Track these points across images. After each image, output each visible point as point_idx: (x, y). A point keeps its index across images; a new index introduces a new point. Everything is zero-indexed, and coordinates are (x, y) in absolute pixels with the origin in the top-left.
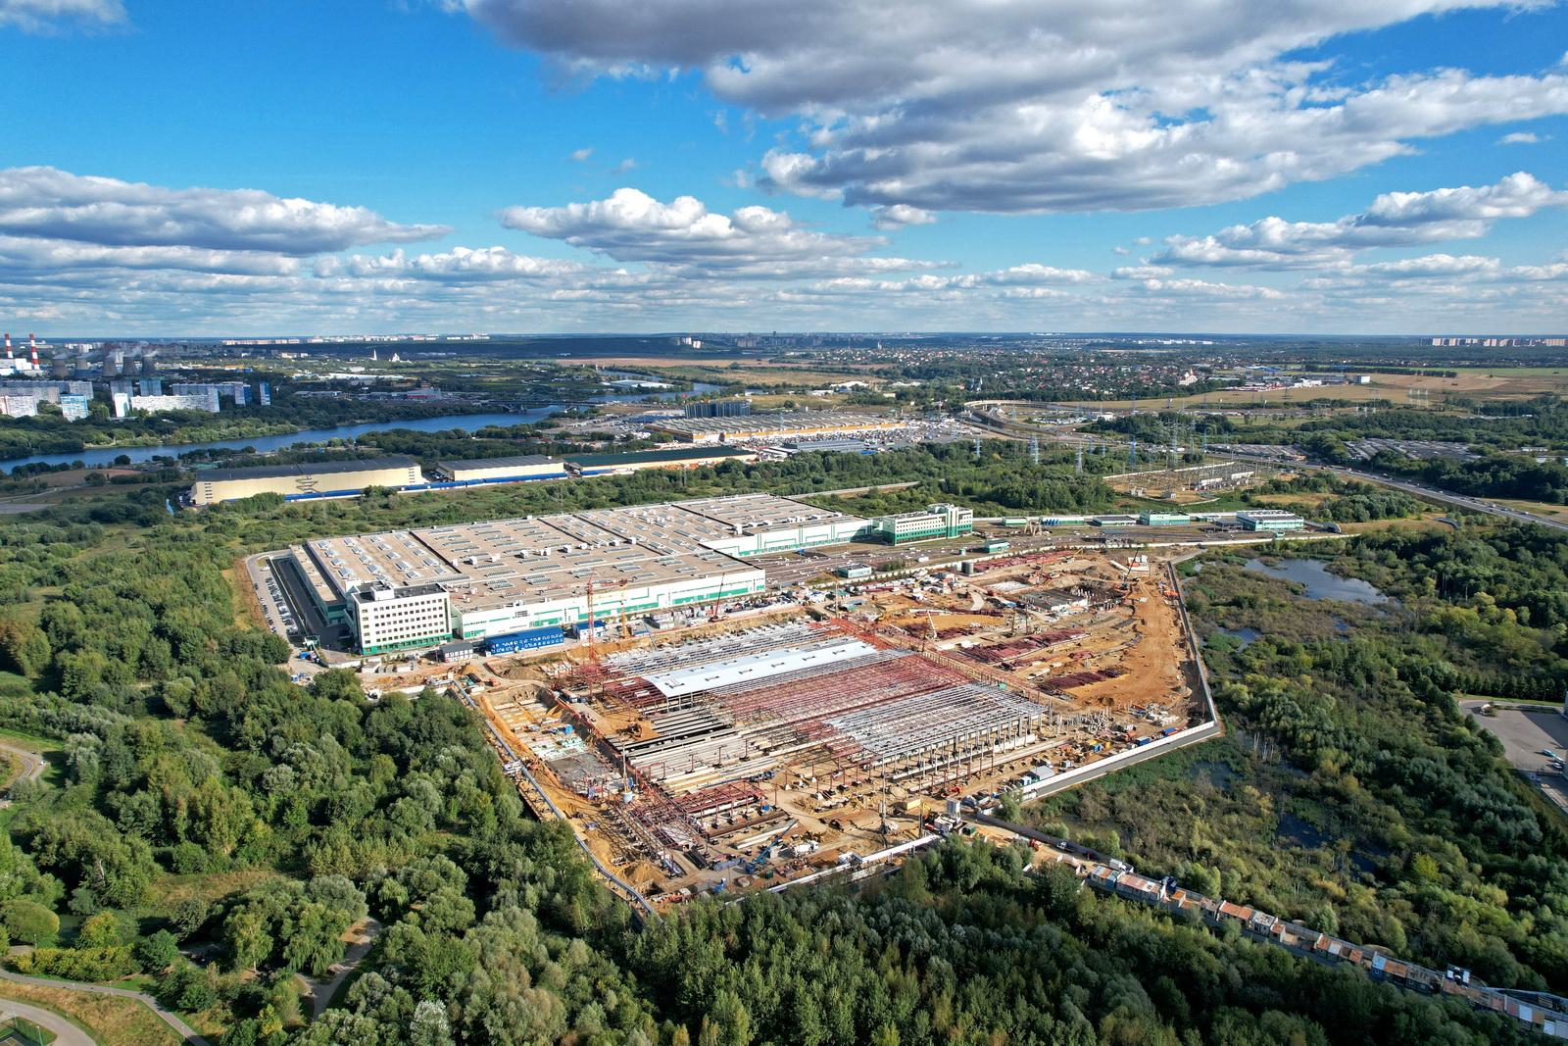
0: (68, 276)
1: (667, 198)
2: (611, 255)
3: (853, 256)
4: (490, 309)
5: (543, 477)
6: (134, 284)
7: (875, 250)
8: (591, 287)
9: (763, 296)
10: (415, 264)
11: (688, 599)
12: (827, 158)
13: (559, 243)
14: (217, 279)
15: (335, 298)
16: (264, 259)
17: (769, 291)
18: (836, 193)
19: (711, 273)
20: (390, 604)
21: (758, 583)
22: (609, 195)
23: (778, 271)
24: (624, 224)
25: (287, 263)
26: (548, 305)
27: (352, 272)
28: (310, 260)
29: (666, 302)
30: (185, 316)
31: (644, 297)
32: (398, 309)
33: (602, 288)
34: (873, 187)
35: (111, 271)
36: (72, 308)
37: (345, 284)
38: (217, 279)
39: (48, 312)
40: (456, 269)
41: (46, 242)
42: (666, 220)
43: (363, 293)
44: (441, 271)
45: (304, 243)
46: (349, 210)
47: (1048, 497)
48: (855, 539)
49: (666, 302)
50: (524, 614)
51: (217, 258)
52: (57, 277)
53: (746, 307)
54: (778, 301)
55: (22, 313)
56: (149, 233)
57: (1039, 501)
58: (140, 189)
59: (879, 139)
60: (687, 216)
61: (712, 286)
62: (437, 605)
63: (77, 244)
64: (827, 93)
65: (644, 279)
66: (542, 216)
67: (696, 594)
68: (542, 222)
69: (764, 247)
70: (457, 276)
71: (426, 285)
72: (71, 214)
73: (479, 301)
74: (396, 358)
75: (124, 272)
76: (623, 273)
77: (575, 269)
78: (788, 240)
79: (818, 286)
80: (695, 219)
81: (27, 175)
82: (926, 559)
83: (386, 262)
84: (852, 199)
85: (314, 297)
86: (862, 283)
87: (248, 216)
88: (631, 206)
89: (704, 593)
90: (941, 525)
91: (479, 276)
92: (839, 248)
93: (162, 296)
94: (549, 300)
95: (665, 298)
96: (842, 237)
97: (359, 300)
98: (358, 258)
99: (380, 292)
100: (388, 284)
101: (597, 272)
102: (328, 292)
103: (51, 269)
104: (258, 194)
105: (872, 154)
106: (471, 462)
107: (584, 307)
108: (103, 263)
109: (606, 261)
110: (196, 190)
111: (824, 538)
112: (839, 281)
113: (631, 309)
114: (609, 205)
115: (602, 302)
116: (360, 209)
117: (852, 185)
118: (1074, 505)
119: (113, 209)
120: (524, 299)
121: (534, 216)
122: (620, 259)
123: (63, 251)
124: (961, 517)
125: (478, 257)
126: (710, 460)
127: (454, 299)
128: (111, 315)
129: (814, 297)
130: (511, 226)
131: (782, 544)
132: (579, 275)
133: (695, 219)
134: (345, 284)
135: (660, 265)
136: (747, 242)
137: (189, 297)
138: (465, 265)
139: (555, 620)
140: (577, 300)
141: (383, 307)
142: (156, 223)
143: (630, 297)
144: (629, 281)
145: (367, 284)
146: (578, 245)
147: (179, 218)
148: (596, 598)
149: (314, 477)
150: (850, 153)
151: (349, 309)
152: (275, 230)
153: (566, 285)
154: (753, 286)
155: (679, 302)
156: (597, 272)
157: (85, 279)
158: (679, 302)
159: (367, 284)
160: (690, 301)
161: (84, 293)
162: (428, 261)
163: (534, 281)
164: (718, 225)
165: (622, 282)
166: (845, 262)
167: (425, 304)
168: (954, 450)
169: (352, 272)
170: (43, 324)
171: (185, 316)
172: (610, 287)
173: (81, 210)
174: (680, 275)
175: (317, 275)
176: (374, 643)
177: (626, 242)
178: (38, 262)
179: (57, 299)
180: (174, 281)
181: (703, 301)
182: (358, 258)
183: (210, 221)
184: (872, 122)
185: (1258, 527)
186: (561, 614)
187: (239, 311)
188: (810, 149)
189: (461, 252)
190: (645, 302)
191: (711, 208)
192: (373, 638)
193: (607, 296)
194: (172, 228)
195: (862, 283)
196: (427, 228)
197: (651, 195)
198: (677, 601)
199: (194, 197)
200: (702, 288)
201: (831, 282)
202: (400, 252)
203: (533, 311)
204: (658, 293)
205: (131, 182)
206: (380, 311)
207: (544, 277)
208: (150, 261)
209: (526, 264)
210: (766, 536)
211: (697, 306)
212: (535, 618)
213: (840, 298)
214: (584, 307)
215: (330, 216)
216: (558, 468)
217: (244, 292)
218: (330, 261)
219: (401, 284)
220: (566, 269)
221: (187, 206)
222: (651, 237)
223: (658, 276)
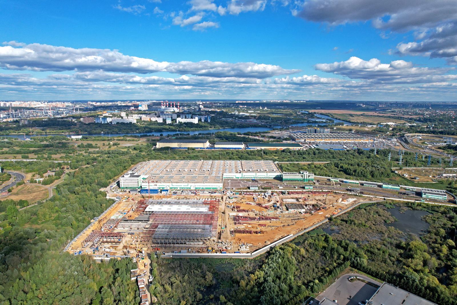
0: (212, 85)
1: (367, 58)
2: (349, 77)
3: (440, 75)
4: (313, 92)
5: (235, 148)
6: (224, 86)
7: (449, 72)
8: (343, 86)
9: (403, 89)
10: (292, 80)
11: (199, 188)
12: (422, 44)
13: (331, 74)
14: (243, 85)
15: (271, 89)
16: (253, 80)
17: (406, 87)
18: (428, 54)
19: (382, 82)
20: (127, 178)
21: (220, 187)
22: (348, 58)
23: (408, 81)
24: (351, 68)
25: (258, 81)
26: (331, 91)
27: (275, 83)
28: (265, 80)
29: (368, 91)
30: (235, 94)
31: (360, 89)
32: (287, 92)
33: (347, 87)
34: (441, 52)
35: (221, 83)
36: (212, 92)
37: (274, 86)
38: (243, 85)
39: (207, 93)
40: (302, 81)
41: (207, 77)
42: (366, 66)
43: (278, 88)
44: (299, 82)
45: (263, 75)
46: (275, 66)
47: (360, 173)
48: (275, 178)
49: (368, 91)
50: (156, 185)
51: (242, 80)
52: (208, 85)
53: (397, 93)
54: (409, 90)
55: (203, 93)
56: (227, 74)
57: (356, 174)
58: (226, 64)
59: (443, 35)
60: (374, 64)
61: (384, 86)
62: (136, 180)
63: (213, 77)
64: (419, 22)
65: (360, 84)
66: (326, 66)
67: (202, 187)
68: (326, 68)
69: (403, 73)
70: (303, 84)
71: (295, 86)
72: (212, 71)
73: (309, 90)
74: (266, 108)
75: (223, 83)
76: (354, 82)
77: (339, 81)
78: (414, 70)
79: (425, 85)
80: (377, 65)
81: (204, 62)
82: (282, 188)
83: (284, 80)
84: (434, 55)
85: (266, 89)
86: (444, 84)
87: (249, 69)
88: (355, 62)
89: (204, 187)
90: (301, 178)
91: (310, 83)
92: (434, 72)
93: (231, 89)
94: (331, 90)
95: (368, 90)
96: (435, 69)
97: (277, 90)
98: (277, 79)
99: (283, 88)
100: (285, 86)
101: (346, 82)
102: (269, 88)
103: (210, 83)
104: (251, 63)
105: (440, 40)
106: (230, 143)
107: (342, 92)
108: (217, 82)
109: (347, 79)
110: (238, 63)
111: (264, 177)
112: (434, 84)
113: (357, 93)
114: (346, 62)
115: (347, 91)
116: (278, 66)
117: (433, 51)
118: (370, 177)
119: (220, 69)
120: (323, 90)
121: (324, 66)
122: (352, 78)
123: (210, 79)
124: (309, 176)
125: (309, 78)
126: (279, 148)
127: (303, 90)
128: (220, 94)
129: (424, 89)
130: (317, 69)
131: (228, 177)
132: (340, 83)
133: (377, 65)
134: (274, 86)
135: (365, 80)
136: (396, 72)
137: (236, 89)
138: (305, 80)
139: (164, 188)
140: (339, 90)
141: (283, 92)
142: (229, 71)
143: (356, 89)
144: (356, 85)
145: (279, 86)
146: (337, 74)
147: (233, 70)
148: (150, 184)
149: (181, 144)
150: (431, 40)
151: (275, 92)
152: (256, 72)
153: (336, 86)
154: (399, 86)
155: (373, 91)
156: (346, 82)
157: (214, 85)
158: (373, 91)
159: (279, 86)
160: (377, 90)
161: (215, 89)
162: (295, 79)
163: (326, 85)
164: (385, 67)
165: (354, 85)
166: (434, 77)
167: (295, 91)
168: (365, 152)
169: (275, 83)
170: (206, 96)
171: (235, 94)
172: (350, 87)
173: (214, 70)
174: (372, 82)
175: (265, 84)
176: (122, 186)
177: (353, 73)
178: (205, 82)
179: (209, 90)
180: (233, 85)
181: (381, 91)
182: (277, 79)
183: (241, 71)
184: (440, 29)
185: (424, 196)
186: (165, 187)
187: (248, 93)
188: (418, 41)
189: (305, 76)
190: (361, 91)
191: (382, 62)
192: (122, 185)
193: (349, 89)
194: (232, 73)
195: (444, 84)
196: (295, 70)
197: (361, 58)
198: (196, 188)
199: (238, 65)
200: (381, 87)
201: (431, 84)
202: (288, 77)
203: (326, 93)
204: (367, 88)
205: (224, 62)
206: (283, 93)
207: (330, 83)
208: (227, 81)
209: (323, 80)
210: (244, 174)
211: (380, 92)
212: (159, 187)
213: (435, 89)
214: (342, 92)
215: (270, 68)
216: (242, 146)
217: (248, 88)
218: (268, 80)
219: (288, 86)
220: (336, 81)
221: (236, 67)
222: (361, 71)
223: (365, 83)
